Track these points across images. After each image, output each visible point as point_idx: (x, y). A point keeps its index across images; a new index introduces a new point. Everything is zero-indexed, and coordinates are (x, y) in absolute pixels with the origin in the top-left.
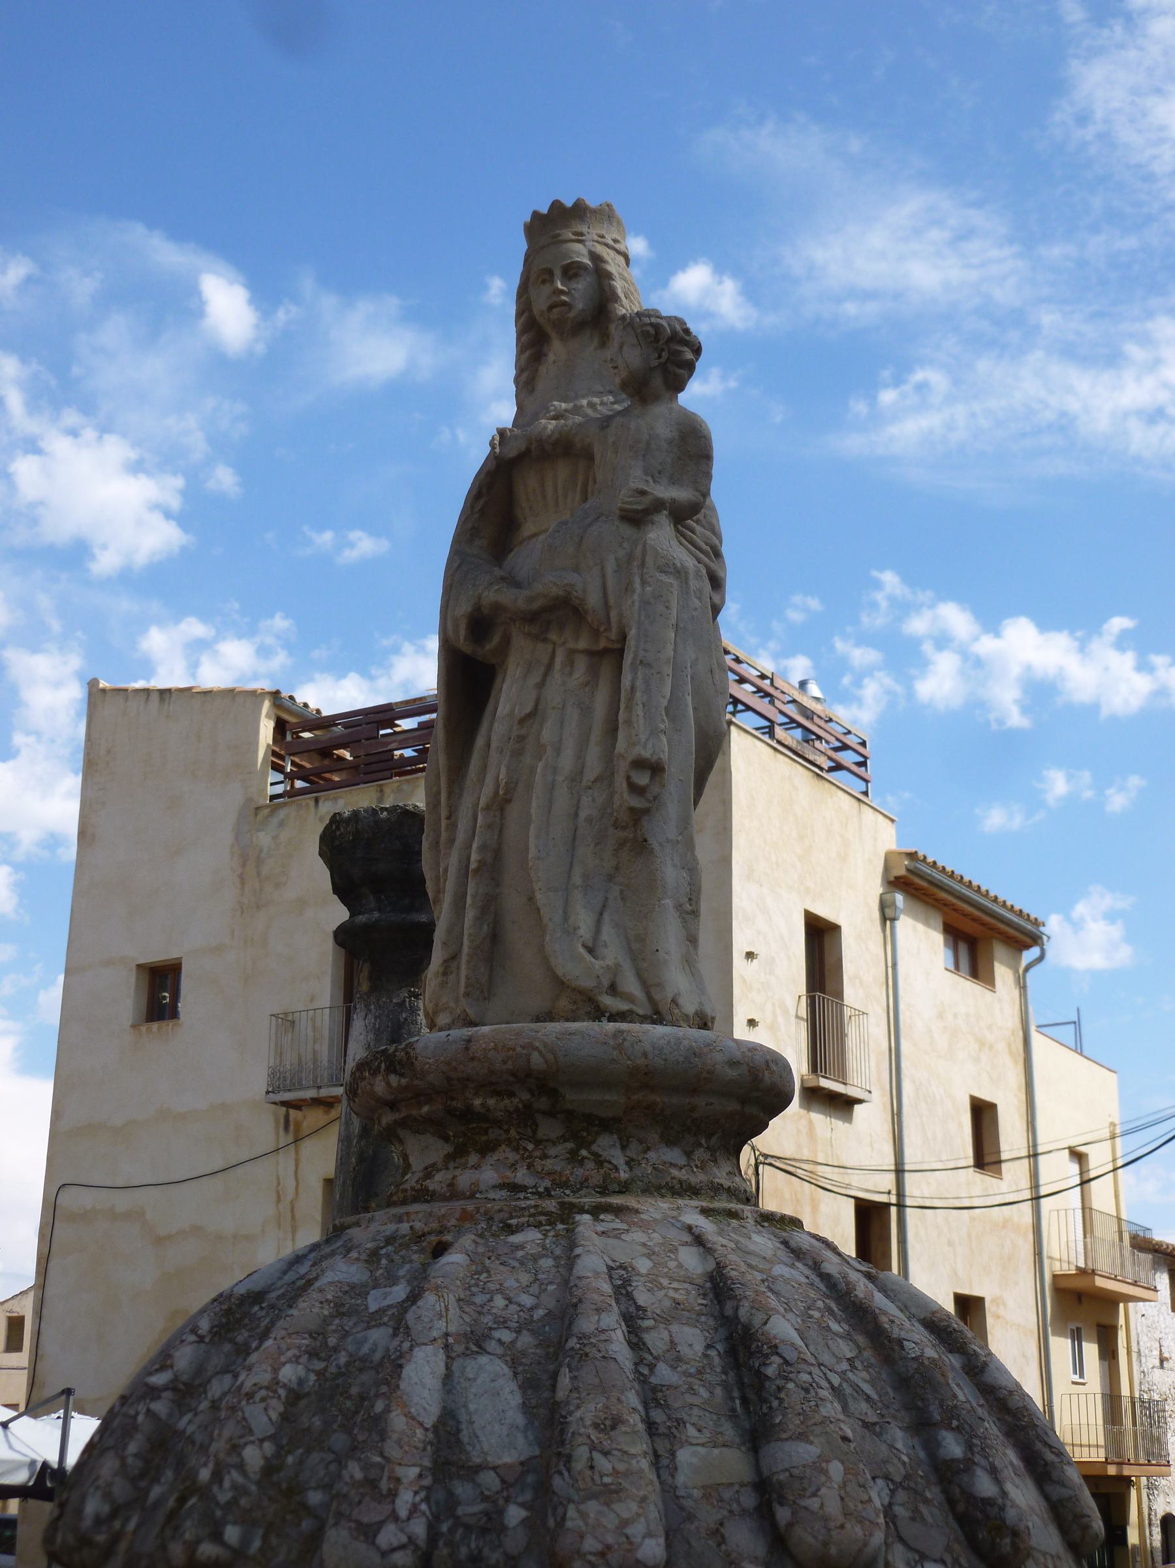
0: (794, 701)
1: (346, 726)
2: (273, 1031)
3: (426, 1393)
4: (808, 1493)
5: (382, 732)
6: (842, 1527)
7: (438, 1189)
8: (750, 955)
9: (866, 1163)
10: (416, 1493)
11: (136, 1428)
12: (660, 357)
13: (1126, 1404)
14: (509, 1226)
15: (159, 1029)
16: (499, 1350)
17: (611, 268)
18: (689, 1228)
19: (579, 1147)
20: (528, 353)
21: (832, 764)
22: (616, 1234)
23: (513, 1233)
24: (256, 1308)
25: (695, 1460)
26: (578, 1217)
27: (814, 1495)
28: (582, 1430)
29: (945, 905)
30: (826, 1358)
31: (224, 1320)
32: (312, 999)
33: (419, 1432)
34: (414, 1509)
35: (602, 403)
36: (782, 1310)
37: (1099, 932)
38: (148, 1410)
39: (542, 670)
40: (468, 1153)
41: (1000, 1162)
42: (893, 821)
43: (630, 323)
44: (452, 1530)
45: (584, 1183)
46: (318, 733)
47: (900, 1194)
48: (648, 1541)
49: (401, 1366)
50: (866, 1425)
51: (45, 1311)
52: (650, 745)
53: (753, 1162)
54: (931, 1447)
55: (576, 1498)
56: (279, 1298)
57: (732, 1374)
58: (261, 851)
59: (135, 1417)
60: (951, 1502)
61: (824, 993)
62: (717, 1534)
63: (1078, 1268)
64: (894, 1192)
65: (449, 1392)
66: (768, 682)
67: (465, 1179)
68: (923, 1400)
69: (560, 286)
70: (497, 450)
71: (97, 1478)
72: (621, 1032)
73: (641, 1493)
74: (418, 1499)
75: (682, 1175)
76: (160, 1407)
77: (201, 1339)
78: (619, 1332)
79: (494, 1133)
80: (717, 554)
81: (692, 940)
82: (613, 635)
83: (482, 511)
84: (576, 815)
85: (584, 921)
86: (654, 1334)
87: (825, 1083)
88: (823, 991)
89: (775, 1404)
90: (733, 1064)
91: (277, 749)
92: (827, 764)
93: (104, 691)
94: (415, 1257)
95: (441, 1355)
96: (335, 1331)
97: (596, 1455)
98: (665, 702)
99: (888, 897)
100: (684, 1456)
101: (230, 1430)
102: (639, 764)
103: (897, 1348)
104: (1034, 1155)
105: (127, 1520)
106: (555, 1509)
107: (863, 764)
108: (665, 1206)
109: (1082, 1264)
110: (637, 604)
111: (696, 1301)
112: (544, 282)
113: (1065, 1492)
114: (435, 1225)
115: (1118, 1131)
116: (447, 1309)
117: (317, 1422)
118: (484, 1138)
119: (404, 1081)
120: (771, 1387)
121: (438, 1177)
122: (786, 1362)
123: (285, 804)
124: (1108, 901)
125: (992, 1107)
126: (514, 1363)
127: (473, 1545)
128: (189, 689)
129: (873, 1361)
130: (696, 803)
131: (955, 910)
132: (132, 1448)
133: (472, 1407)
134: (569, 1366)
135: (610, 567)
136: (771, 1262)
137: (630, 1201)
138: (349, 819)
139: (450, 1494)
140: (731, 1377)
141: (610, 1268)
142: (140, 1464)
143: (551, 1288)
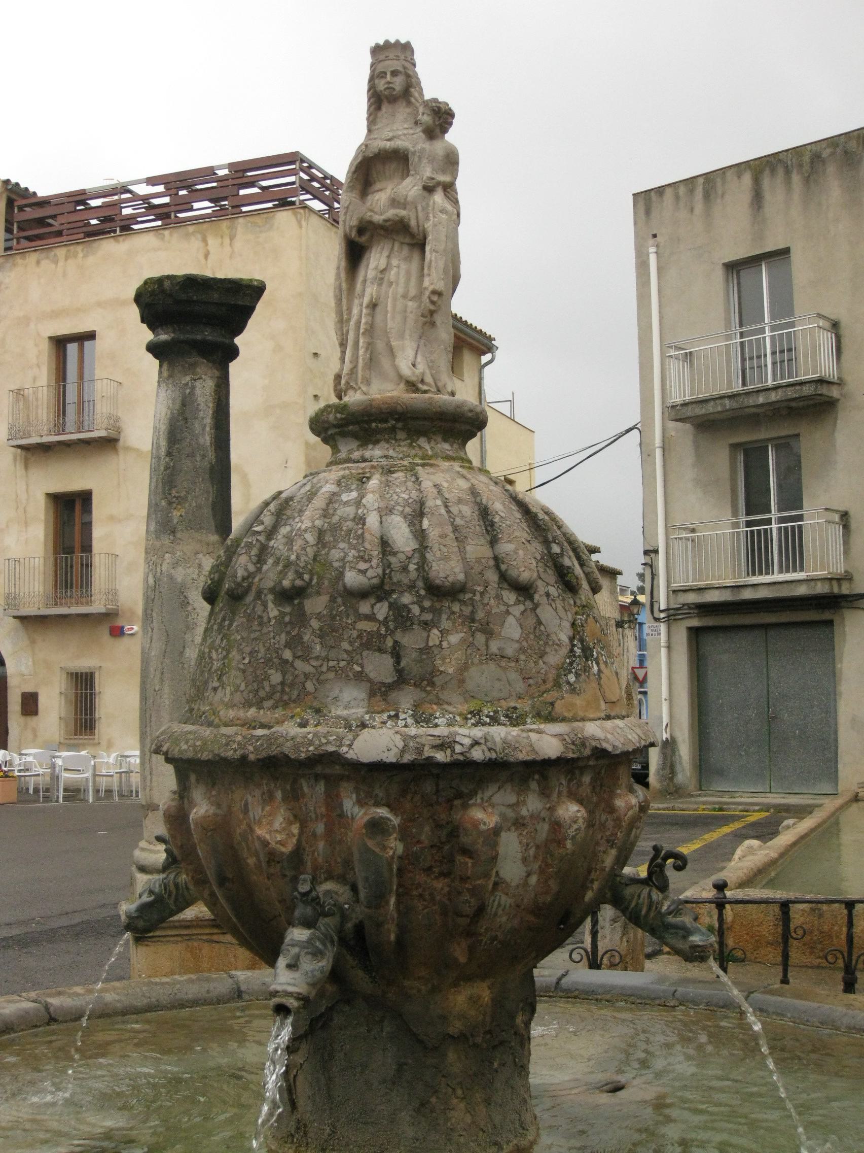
5: (78, 208)
22: (434, 474)
43: (426, 104)
44: (390, 573)
54: (549, 549)
67: (368, 454)
75: (450, 453)
79: (378, 436)
83: (356, 179)
102: (434, 292)
113: (590, 570)
126: (405, 517)
135: (419, 208)
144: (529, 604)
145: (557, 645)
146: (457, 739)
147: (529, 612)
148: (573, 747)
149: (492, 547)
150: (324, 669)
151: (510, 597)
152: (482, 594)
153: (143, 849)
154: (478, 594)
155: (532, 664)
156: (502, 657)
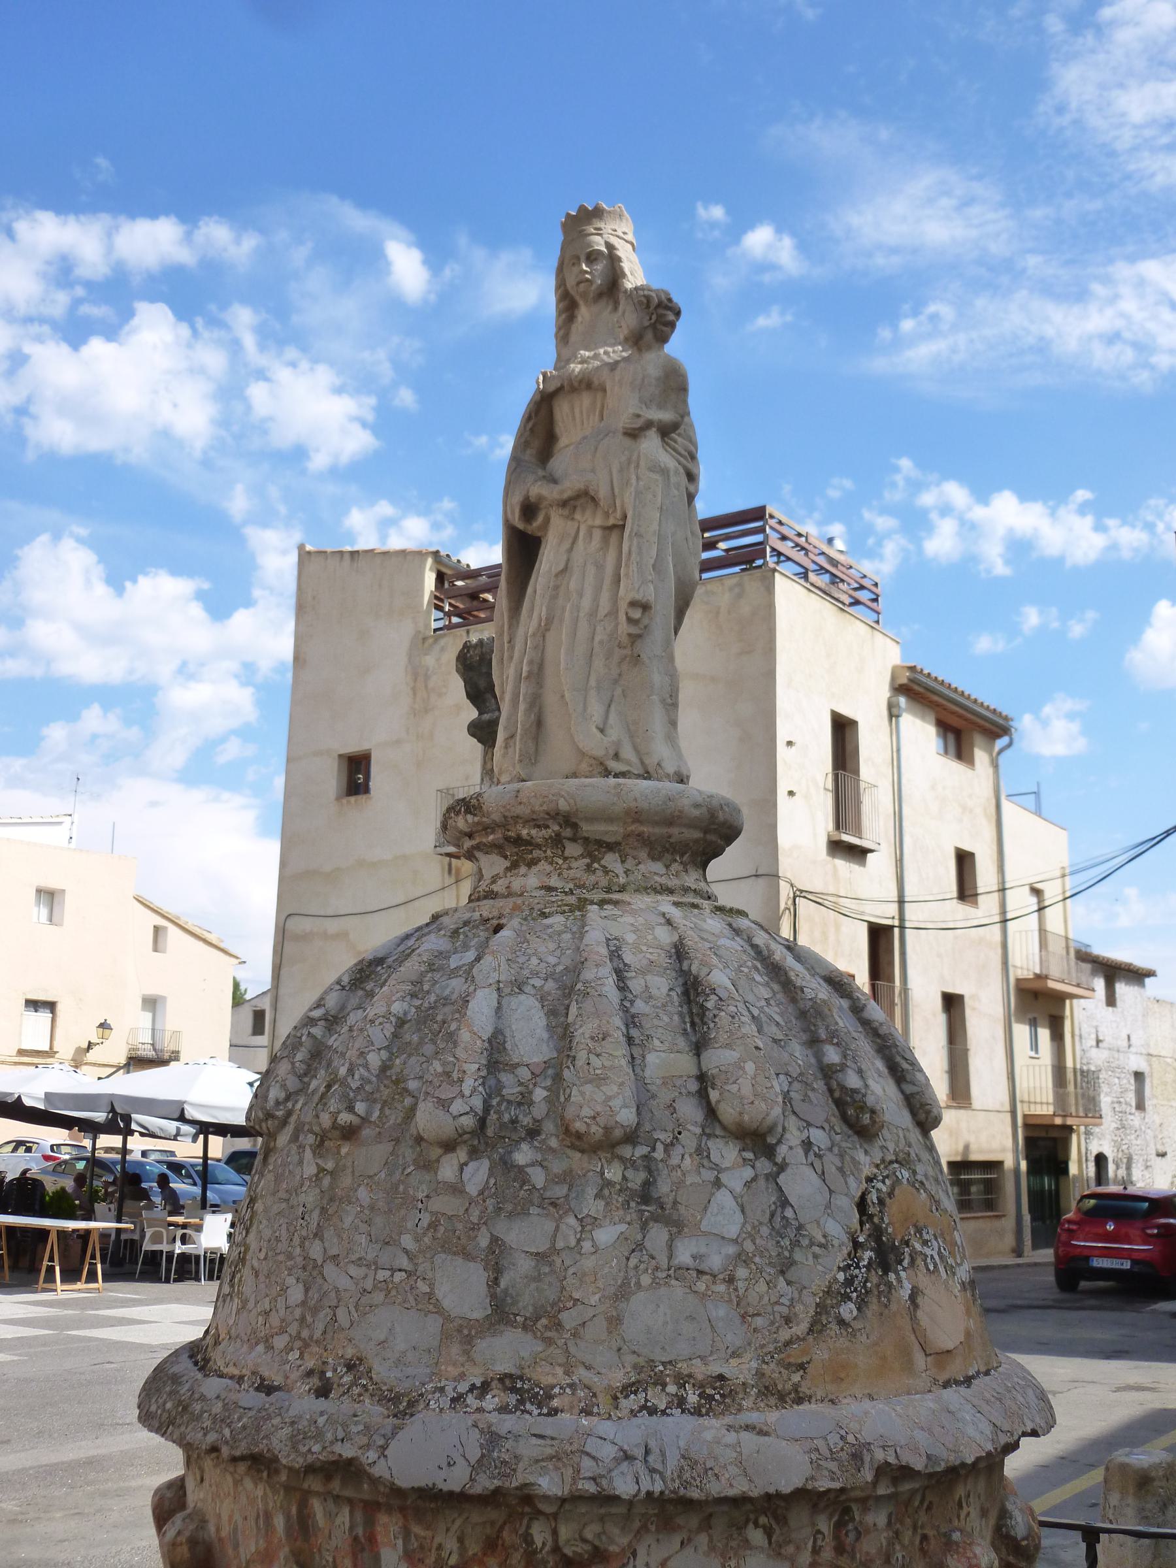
0: (823, 553)
1: (489, 576)
2: (439, 800)
3: (484, 1019)
4: (731, 1081)
6: (752, 1103)
7: (500, 891)
8: (790, 743)
9: (875, 896)
10: (476, 1080)
11: (301, 1044)
12: (651, 319)
13: (1070, 1075)
14: (544, 913)
15: (356, 801)
16: (533, 992)
17: (620, 253)
18: (664, 915)
19: (593, 862)
20: (564, 316)
21: (853, 601)
22: (614, 918)
23: (546, 917)
24: (379, 968)
25: (657, 1061)
26: (589, 907)
27: (734, 1083)
28: (583, 1041)
29: (938, 706)
30: (750, 998)
31: (358, 976)
32: (467, 778)
33: (479, 1042)
34: (474, 1090)
35: (614, 352)
36: (721, 967)
37: (1060, 727)
38: (309, 1033)
39: (570, 540)
40: (519, 866)
41: (977, 895)
42: (898, 643)
43: (630, 295)
44: (499, 1104)
45: (595, 886)
46: (467, 581)
47: (902, 919)
48: (623, 1110)
49: (468, 1001)
50: (775, 1041)
51: (279, 1005)
52: (641, 590)
53: (791, 895)
54: (819, 1056)
55: (578, 1082)
56: (394, 961)
57: (685, 1007)
58: (428, 670)
59: (300, 1038)
60: (831, 1091)
61: (845, 770)
62: (671, 1108)
63: (1035, 974)
64: (897, 917)
65: (499, 1018)
66: (803, 539)
67: (517, 884)
68: (815, 1025)
69: (584, 267)
70: (541, 387)
71: (277, 1076)
72: (619, 785)
73: (620, 1080)
74: (477, 1084)
75: (663, 880)
76: (317, 1031)
77: (343, 988)
78: (610, 979)
79: (537, 853)
80: (693, 457)
81: (673, 723)
82: (619, 514)
83: (532, 430)
84: (593, 638)
85: (596, 709)
86: (635, 981)
87: (846, 838)
88: (844, 769)
89: (712, 1025)
90: (697, 806)
91: (438, 594)
92: (847, 600)
93: (309, 553)
94: (482, 934)
95: (495, 995)
96: (429, 981)
97: (592, 1057)
98: (652, 561)
99: (894, 699)
100: (651, 1058)
101: (359, 1043)
102: (633, 604)
103: (799, 992)
104: (1002, 890)
105: (296, 1102)
106: (564, 1090)
107: (876, 600)
108: (649, 900)
109: (1038, 971)
110: (633, 494)
111: (664, 960)
112: (573, 264)
114: (496, 914)
115: (1067, 871)
116: (499, 966)
117: (415, 1038)
118: (530, 856)
119: (476, 819)
120: (710, 1015)
121: (500, 882)
122: (721, 999)
123: (445, 635)
124: (1069, 705)
125: (971, 855)
126: (542, 999)
127: (512, 1113)
128: (372, 551)
129: (783, 1000)
130: (676, 633)
131: (945, 709)
132: (299, 1056)
133: (514, 1027)
134: (577, 1001)
136: (718, 937)
137: (624, 897)
138: (476, 645)
139: (499, 1081)
140: (685, 1009)
141: (608, 940)
142: (304, 1066)
143: (568, 952)
144: (764, 1165)
145: (820, 1246)
146: (588, 1449)
147: (762, 1182)
148: (833, 1466)
149: (698, 1055)
150: (369, 1285)
151: (726, 1153)
152: (668, 1147)
153: (218, 1530)
154: (660, 1147)
155: (762, 1287)
156: (700, 1272)
